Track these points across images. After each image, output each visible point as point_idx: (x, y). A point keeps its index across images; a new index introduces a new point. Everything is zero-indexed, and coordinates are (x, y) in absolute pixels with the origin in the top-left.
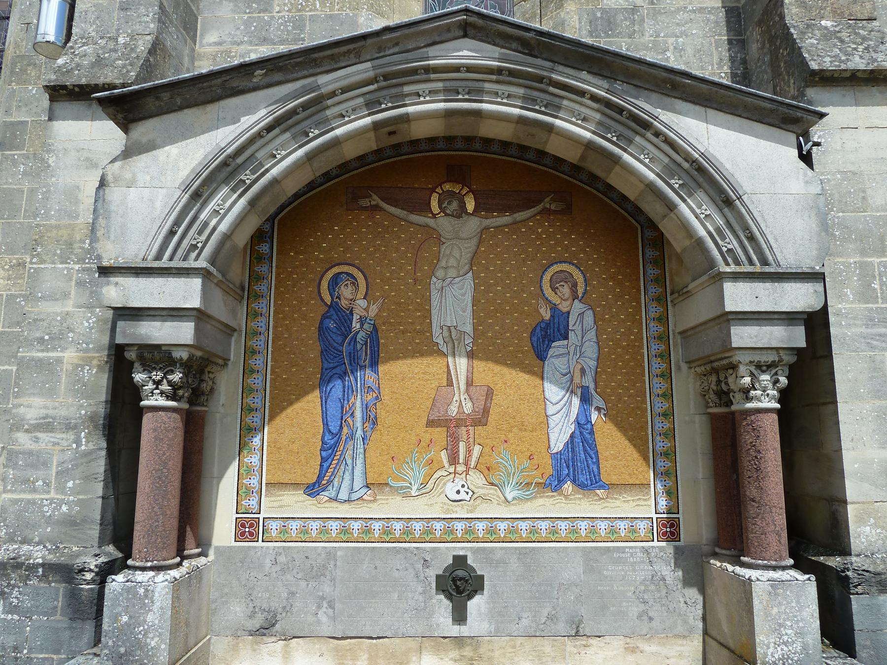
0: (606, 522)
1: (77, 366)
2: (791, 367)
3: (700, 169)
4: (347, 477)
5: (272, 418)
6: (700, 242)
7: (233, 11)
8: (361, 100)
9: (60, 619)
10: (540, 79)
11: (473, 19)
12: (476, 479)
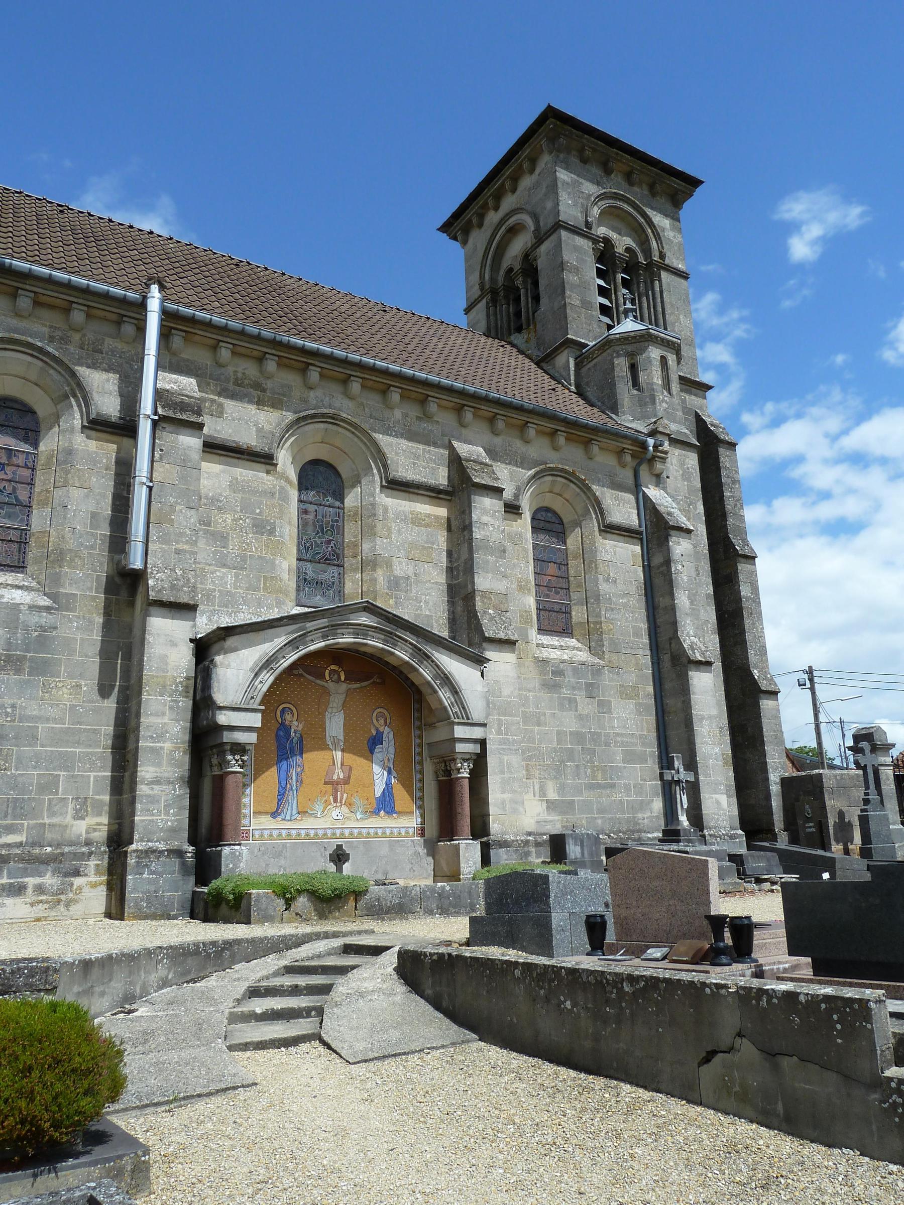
0: (397, 829)
1: (172, 751)
2: (474, 760)
3: (447, 678)
4: (290, 808)
5: (255, 779)
6: (445, 708)
7: (206, 544)
8: (320, 634)
9: (177, 876)
10: (391, 633)
11: (370, 606)
12: (345, 809)
